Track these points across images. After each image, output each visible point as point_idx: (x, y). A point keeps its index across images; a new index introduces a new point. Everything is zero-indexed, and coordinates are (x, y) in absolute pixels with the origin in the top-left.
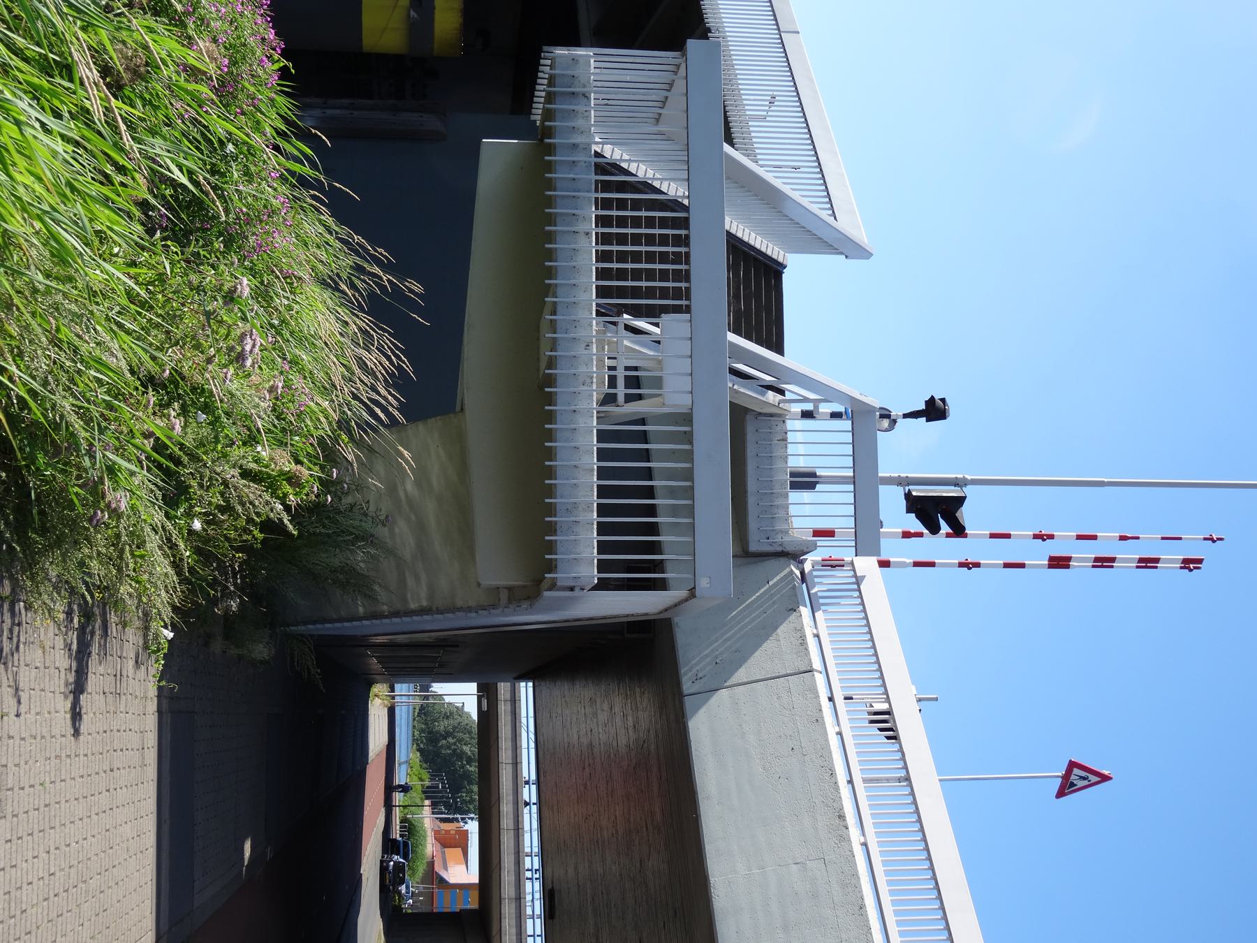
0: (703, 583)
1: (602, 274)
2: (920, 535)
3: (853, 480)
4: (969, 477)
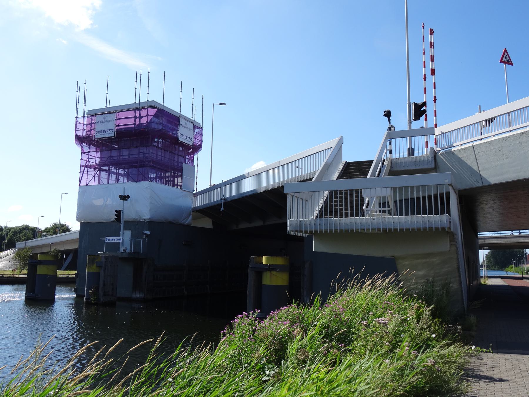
0: (447, 182)
1: (352, 215)
2: (426, 115)
3: (410, 137)
4: (408, 102)
